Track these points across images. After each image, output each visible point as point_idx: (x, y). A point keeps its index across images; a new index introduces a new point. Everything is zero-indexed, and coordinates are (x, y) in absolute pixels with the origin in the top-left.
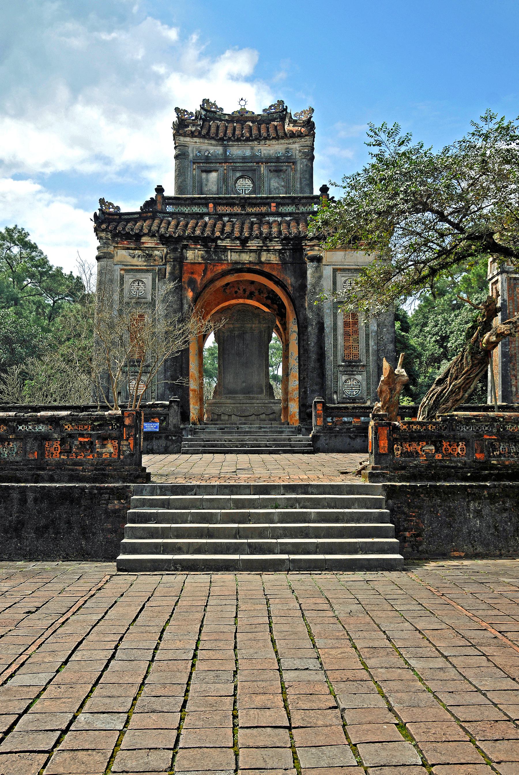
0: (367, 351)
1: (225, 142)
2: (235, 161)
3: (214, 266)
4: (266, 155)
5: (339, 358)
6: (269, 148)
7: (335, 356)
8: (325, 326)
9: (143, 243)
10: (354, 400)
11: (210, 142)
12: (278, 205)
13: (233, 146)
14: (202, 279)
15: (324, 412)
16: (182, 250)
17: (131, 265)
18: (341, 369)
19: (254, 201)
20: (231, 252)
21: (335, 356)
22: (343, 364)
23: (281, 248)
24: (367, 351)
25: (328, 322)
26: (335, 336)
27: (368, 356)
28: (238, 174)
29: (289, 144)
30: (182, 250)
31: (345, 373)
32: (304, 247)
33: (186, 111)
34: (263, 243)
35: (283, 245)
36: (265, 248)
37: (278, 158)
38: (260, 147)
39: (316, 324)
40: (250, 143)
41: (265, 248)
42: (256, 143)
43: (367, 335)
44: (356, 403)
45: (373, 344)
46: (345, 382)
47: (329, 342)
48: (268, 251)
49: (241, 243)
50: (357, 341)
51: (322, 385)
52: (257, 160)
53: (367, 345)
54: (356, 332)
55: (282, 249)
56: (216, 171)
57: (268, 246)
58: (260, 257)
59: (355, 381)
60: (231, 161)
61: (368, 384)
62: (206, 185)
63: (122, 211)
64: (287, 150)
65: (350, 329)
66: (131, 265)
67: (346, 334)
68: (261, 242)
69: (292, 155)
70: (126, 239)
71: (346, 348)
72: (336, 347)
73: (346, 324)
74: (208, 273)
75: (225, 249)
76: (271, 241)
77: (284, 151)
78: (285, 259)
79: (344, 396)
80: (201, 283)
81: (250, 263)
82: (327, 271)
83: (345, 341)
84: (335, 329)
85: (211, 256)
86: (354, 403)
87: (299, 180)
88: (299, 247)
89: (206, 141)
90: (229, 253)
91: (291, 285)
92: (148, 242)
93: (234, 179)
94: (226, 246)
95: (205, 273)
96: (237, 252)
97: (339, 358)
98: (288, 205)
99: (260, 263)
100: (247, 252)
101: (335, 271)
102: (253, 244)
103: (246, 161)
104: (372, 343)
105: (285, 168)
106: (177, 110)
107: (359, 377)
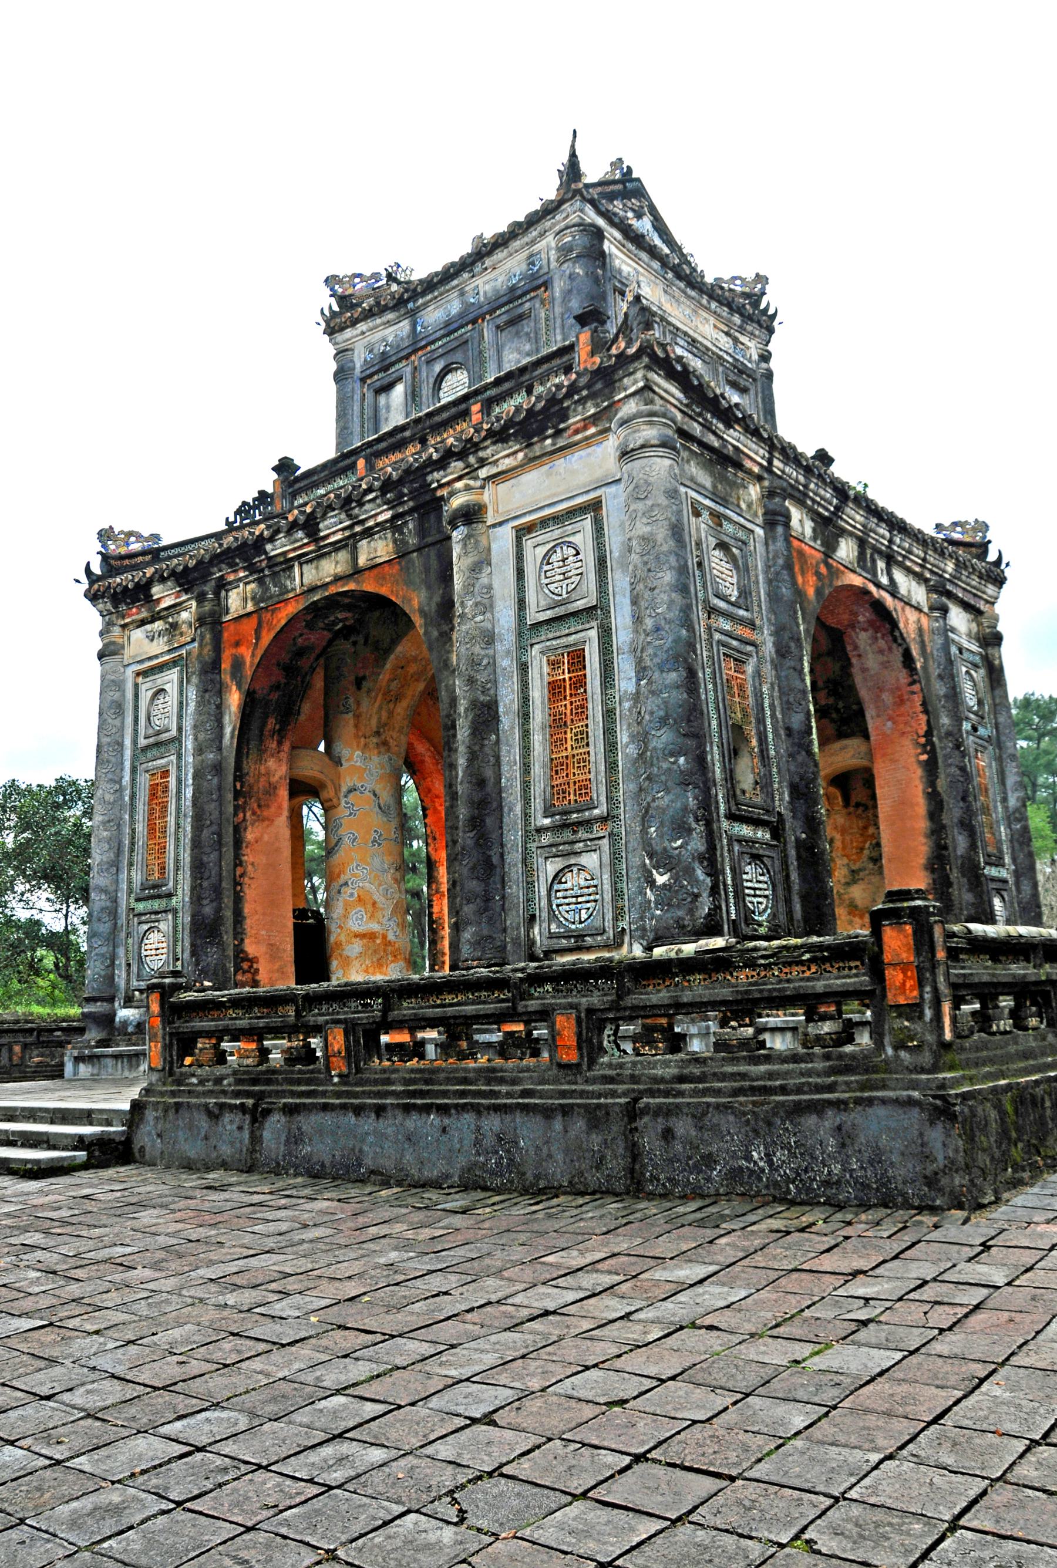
0: (611, 766)
1: (410, 305)
2: (432, 338)
3: (273, 611)
4: (489, 295)
5: (537, 804)
6: (492, 276)
7: (526, 800)
8: (501, 709)
9: (159, 600)
10: (579, 942)
11: (385, 319)
12: (488, 405)
13: (426, 305)
14: (253, 655)
15: (163, 1022)
16: (217, 594)
17: (150, 659)
18: (546, 839)
19: (438, 419)
20: (301, 565)
21: (526, 800)
22: (547, 821)
23: (388, 515)
24: (611, 766)
25: (508, 698)
26: (526, 734)
27: (612, 785)
28: (438, 367)
29: (533, 242)
30: (217, 594)
31: (552, 851)
32: (439, 493)
33: (359, 275)
34: (350, 517)
35: (392, 505)
36: (358, 529)
37: (513, 289)
38: (479, 281)
39: (467, 710)
40: (455, 282)
41: (358, 529)
42: (466, 275)
43: (609, 714)
44: (589, 949)
45: (625, 739)
46: (557, 877)
47: (511, 755)
48: (368, 533)
49: (308, 535)
50: (583, 738)
51: (487, 899)
52: (471, 317)
53: (611, 747)
54: (581, 710)
55: (394, 518)
56: (399, 379)
57: (362, 522)
58: (355, 558)
59: (583, 875)
60: (423, 343)
61: (616, 877)
62: (387, 419)
63: (166, 542)
64: (531, 260)
65: (565, 706)
66: (150, 659)
67: (557, 724)
68: (343, 516)
69: (540, 268)
70: (133, 603)
71: (556, 767)
72: (525, 766)
73: (555, 689)
74: (264, 633)
75: (286, 564)
76: (361, 504)
77: (524, 267)
78: (404, 542)
79: (554, 928)
80: (252, 663)
81: (338, 579)
82: (503, 541)
83: (556, 742)
84: (525, 716)
85: (268, 589)
86: (578, 949)
87: (559, 322)
88: (428, 498)
89: (379, 321)
90: (296, 569)
91: (422, 612)
92: (165, 595)
93: (432, 380)
94: (285, 553)
95: (258, 639)
96: (311, 561)
97: (537, 804)
98: (509, 394)
99: (357, 572)
100: (329, 553)
101: (523, 532)
102: (333, 527)
103: (451, 328)
104: (623, 737)
105: (527, 305)
106: (331, 281)
107: (590, 860)
